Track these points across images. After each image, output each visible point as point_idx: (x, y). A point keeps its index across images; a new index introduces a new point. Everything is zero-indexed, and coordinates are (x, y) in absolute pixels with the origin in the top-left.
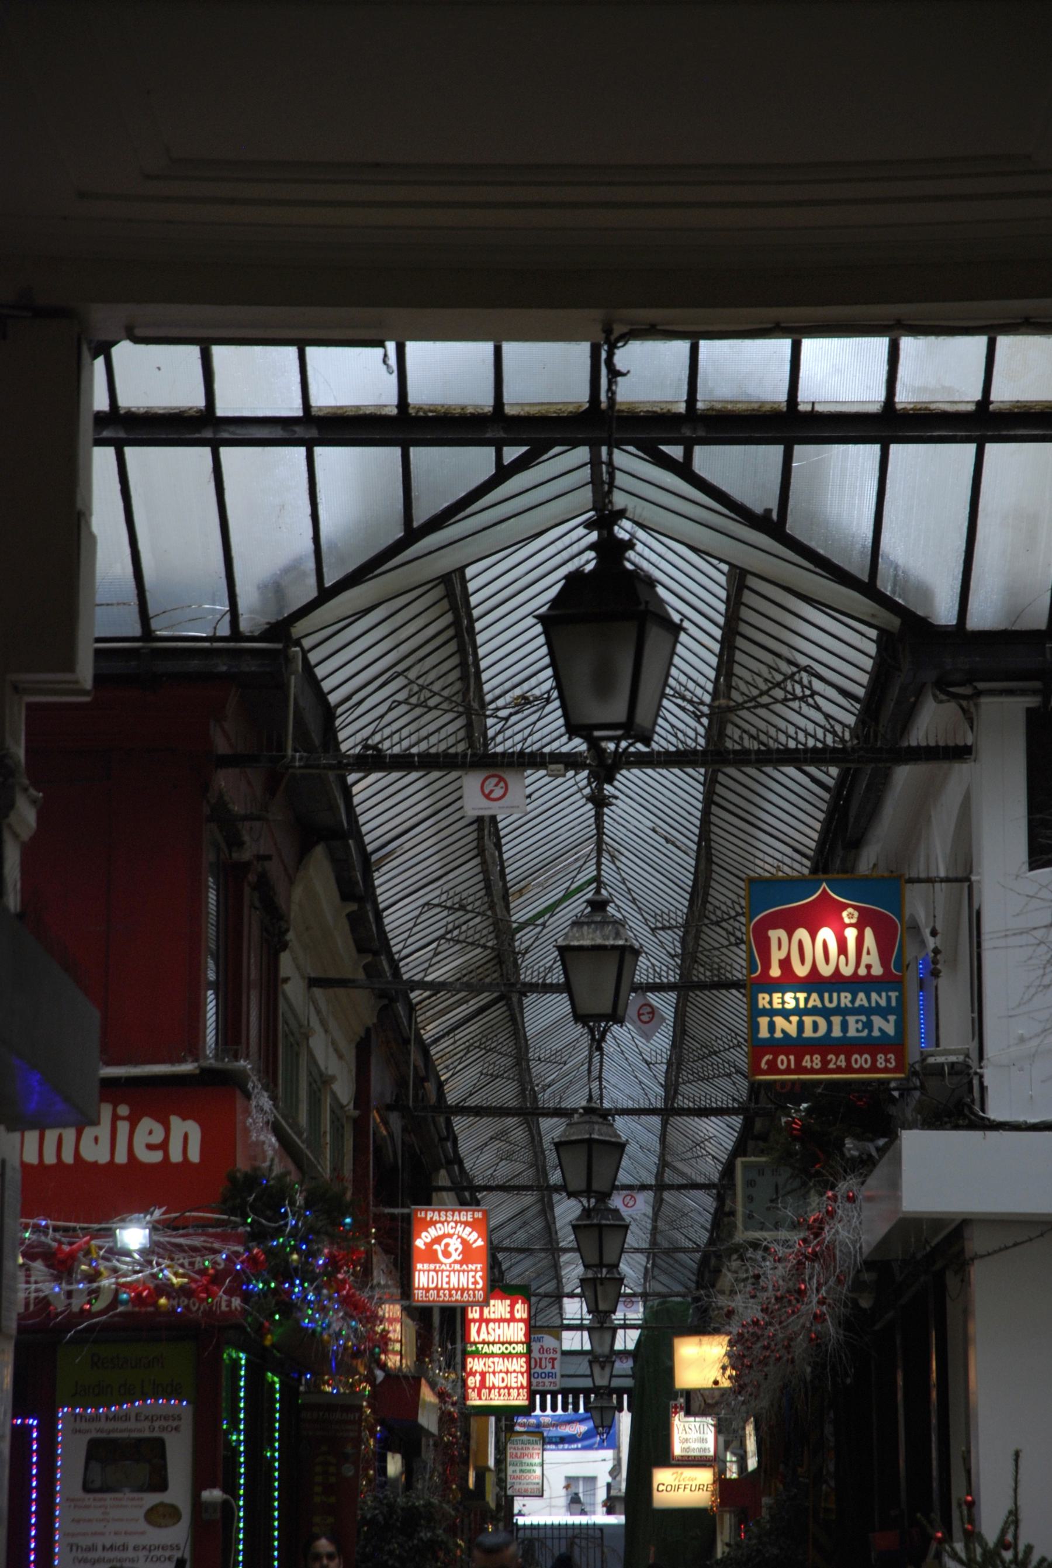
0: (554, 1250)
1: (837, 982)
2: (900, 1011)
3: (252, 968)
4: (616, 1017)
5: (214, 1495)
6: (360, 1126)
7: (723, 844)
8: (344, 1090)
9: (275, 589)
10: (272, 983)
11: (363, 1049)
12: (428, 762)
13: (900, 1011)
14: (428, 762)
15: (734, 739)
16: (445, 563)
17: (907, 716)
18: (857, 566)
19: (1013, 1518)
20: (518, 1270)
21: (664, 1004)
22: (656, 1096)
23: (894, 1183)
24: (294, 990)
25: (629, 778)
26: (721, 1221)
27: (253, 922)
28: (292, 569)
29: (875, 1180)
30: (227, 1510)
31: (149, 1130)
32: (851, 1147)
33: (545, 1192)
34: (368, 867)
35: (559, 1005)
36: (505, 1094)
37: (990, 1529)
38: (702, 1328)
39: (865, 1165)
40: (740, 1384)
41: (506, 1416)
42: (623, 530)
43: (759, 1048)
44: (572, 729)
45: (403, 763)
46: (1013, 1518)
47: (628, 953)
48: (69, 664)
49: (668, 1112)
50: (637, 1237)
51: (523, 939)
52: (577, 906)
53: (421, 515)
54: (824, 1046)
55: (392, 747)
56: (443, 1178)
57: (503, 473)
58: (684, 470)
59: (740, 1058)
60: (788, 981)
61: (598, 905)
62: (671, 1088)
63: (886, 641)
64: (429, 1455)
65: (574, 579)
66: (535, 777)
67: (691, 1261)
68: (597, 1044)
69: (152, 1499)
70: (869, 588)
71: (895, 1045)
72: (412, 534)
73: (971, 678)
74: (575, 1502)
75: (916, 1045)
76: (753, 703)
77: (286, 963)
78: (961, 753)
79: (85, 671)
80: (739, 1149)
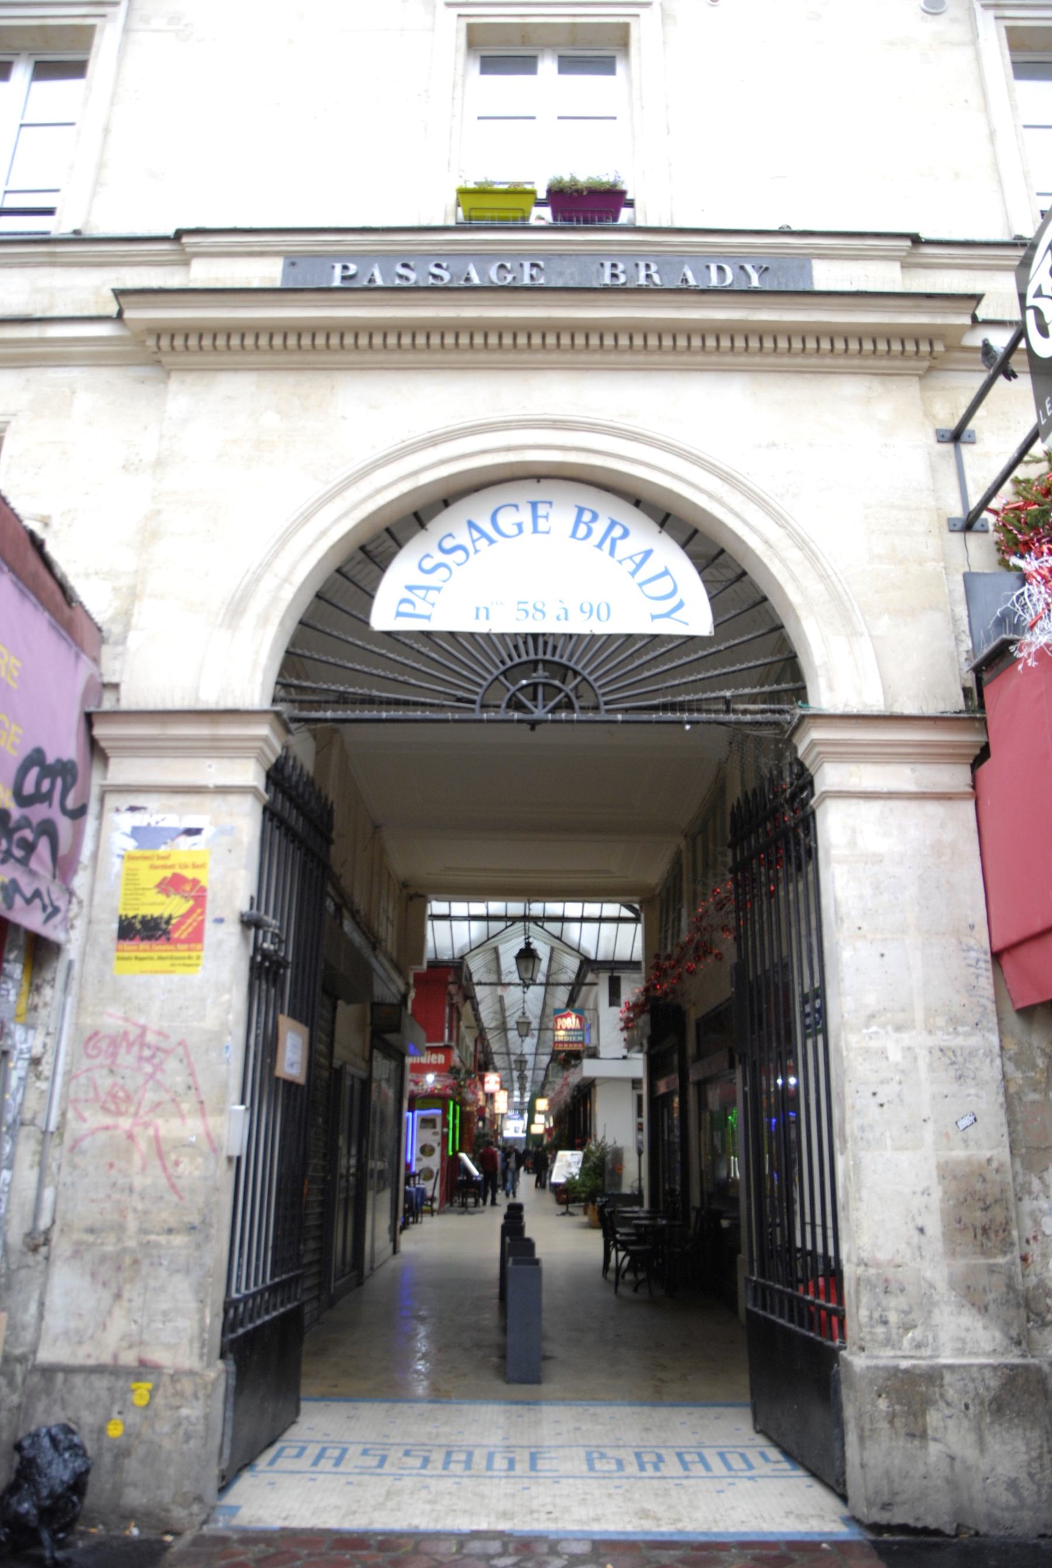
0: (512, 1081)
1: (571, 1030)
2: (583, 1036)
3: (455, 1024)
4: (526, 1035)
5: (445, 1130)
6: (475, 1056)
7: (548, 1001)
8: (472, 1048)
9: (461, 949)
10: (458, 1027)
11: (476, 1041)
12: (490, 984)
13: (583, 1036)
14: (490, 984)
15: (551, 980)
16: (494, 945)
17: (585, 976)
18: (576, 947)
19: (604, 1137)
20: (506, 1085)
21: (536, 1033)
22: (533, 1051)
23: (581, 1069)
24: (463, 1029)
25: (532, 988)
26: (546, 1076)
27: (455, 1016)
28: (465, 946)
29: (578, 1069)
30: (448, 1134)
31: (434, 1056)
32: (573, 1062)
33: (511, 1070)
34: (478, 1004)
35: (516, 1033)
36: (504, 1050)
37: (599, 1138)
38: (542, 1096)
39: (576, 1066)
40: (550, 1109)
41: (503, 1115)
42: (531, 940)
43: (555, 1043)
44: (521, 979)
45: (485, 984)
46: (604, 1137)
47: (529, 1023)
48: (421, 963)
49: (536, 1054)
50: (529, 1079)
51: (508, 1019)
52: (519, 1013)
53: (491, 935)
54: (568, 1042)
55: (483, 981)
56: (491, 1066)
57: (507, 927)
58: (542, 927)
59: (551, 1044)
60: (561, 1029)
61: (524, 1013)
62: (537, 1049)
63: (582, 963)
64: (487, 1122)
65: (521, 950)
66: (512, 988)
67: (540, 1084)
68: (523, 1041)
69: (433, 1130)
70: (578, 951)
71: (582, 1042)
72: (489, 939)
73: (598, 969)
74: (516, 1131)
75: (587, 1042)
76: (555, 973)
77: (462, 1023)
78: (595, 984)
79: (425, 966)
80: (550, 1062)
